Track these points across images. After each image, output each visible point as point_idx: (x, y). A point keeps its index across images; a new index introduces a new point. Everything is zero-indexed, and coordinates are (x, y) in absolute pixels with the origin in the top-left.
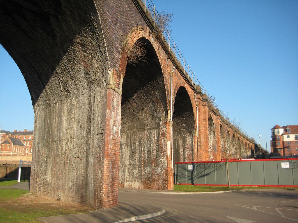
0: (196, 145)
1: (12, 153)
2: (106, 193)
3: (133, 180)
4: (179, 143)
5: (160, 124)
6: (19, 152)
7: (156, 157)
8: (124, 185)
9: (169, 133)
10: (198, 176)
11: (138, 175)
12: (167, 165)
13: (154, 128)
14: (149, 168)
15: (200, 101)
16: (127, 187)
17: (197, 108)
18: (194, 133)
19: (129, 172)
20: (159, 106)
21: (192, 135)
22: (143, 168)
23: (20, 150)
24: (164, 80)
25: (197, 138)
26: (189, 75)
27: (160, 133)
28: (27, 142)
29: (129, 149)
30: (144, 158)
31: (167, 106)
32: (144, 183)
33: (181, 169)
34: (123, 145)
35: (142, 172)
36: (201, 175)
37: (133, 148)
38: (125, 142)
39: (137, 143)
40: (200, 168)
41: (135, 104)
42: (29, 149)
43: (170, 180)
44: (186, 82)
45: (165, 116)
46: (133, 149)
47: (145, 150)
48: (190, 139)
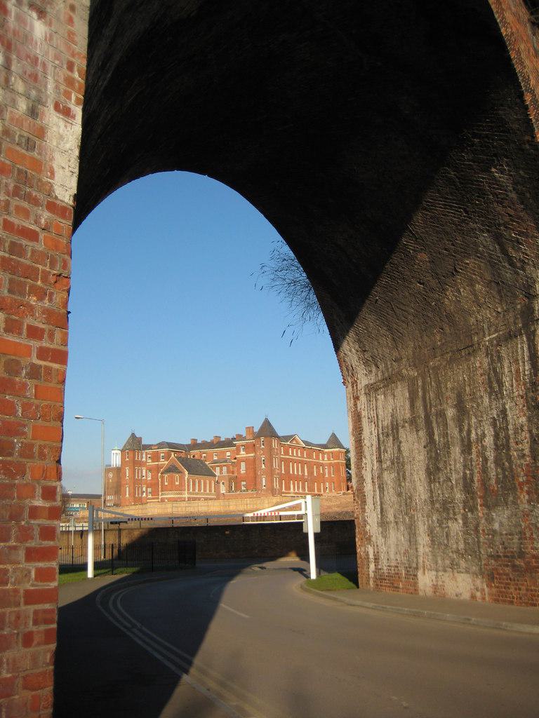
1: (186, 496)
3: (448, 562)
6: (202, 491)
8: (415, 584)
11: (466, 543)
13: (510, 336)
14: (507, 513)
16: (429, 592)
19: (431, 532)
20: (520, 233)
23: (199, 486)
24: (523, 101)
28: (221, 467)
29: (423, 442)
30: (484, 470)
32: (491, 577)
34: (403, 427)
35: (480, 528)
37: (436, 433)
38: (408, 416)
41: (424, 257)
42: (227, 483)
46: (436, 437)
47: (484, 435)
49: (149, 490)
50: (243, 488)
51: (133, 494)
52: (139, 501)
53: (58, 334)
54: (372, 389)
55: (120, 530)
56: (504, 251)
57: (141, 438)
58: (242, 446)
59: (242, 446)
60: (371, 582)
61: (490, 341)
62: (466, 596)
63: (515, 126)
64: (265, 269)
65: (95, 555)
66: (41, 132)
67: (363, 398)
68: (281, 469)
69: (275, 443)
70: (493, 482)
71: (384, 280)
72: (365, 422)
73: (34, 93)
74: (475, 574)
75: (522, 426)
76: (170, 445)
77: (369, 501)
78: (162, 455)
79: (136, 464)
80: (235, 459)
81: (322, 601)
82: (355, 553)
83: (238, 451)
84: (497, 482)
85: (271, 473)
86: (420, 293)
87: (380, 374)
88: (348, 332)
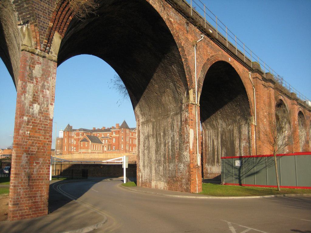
0: (253, 135)
2: (12, 198)
4: (234, 133)
5: (182, 108)
6: (97, 149)
7: (179, 150)
8: (151, 185)
9: (192, 118)
10: (246, 175)
11: (163, 173)
12: (189, 161)
13: (176, 114)
15: (259, 81)
16: (154, 188)
17: (253, 89)
18: (250, 120)
19: (155, 170)
20: (180, 85)
21: (249, 123)
22: (167, 164)
23: (98, 148)
25: (255, 126)
26: (238, 47)
27: (183, 120)
31: (188, 84)
32: (168, 183)
33: (227, 166)
36: (249, 173)
39: (162, 134)
40: (249, 164)
41: (157, 86)
43: (193, 180)
44: (232, 56)
45: (187, 97)
46: (158, 141)
47: (169, 142)
48: (247, 128)
49: (75, 148)
50: (114, 149)
51: (68, 150)
52: (70, 152)
53: (51, 138)
54: (143, 123)
55: (61, 164)
56: (176, 89)
57: (72, 126)
58: (114, 131)
59: (114, 131)
60: (140, 184)
61: (172, 114)
62: (162, 188)
63: (177, 56)
64: (112, 81)
65: (52, 174)
66: (48, 109)
67: (141, 126)
68: (130, 142)
69: (128, 131)
70: (170, 155)
71: (146, 91)
72: (141, 133)
73: (47, 103)
74: (165, 182)
75: (178, 140)
76: (84, 130)
77: (141, 159)
78: (81, 134)
79: (69, 137)
80: (111, 137)
81: (124, 189)
82: (136, 175)
83: (112, 133)
84: (171, 155)
85: (125, 143)
86: (156, 96)
87: (145, 119)
88: (137, 104)
